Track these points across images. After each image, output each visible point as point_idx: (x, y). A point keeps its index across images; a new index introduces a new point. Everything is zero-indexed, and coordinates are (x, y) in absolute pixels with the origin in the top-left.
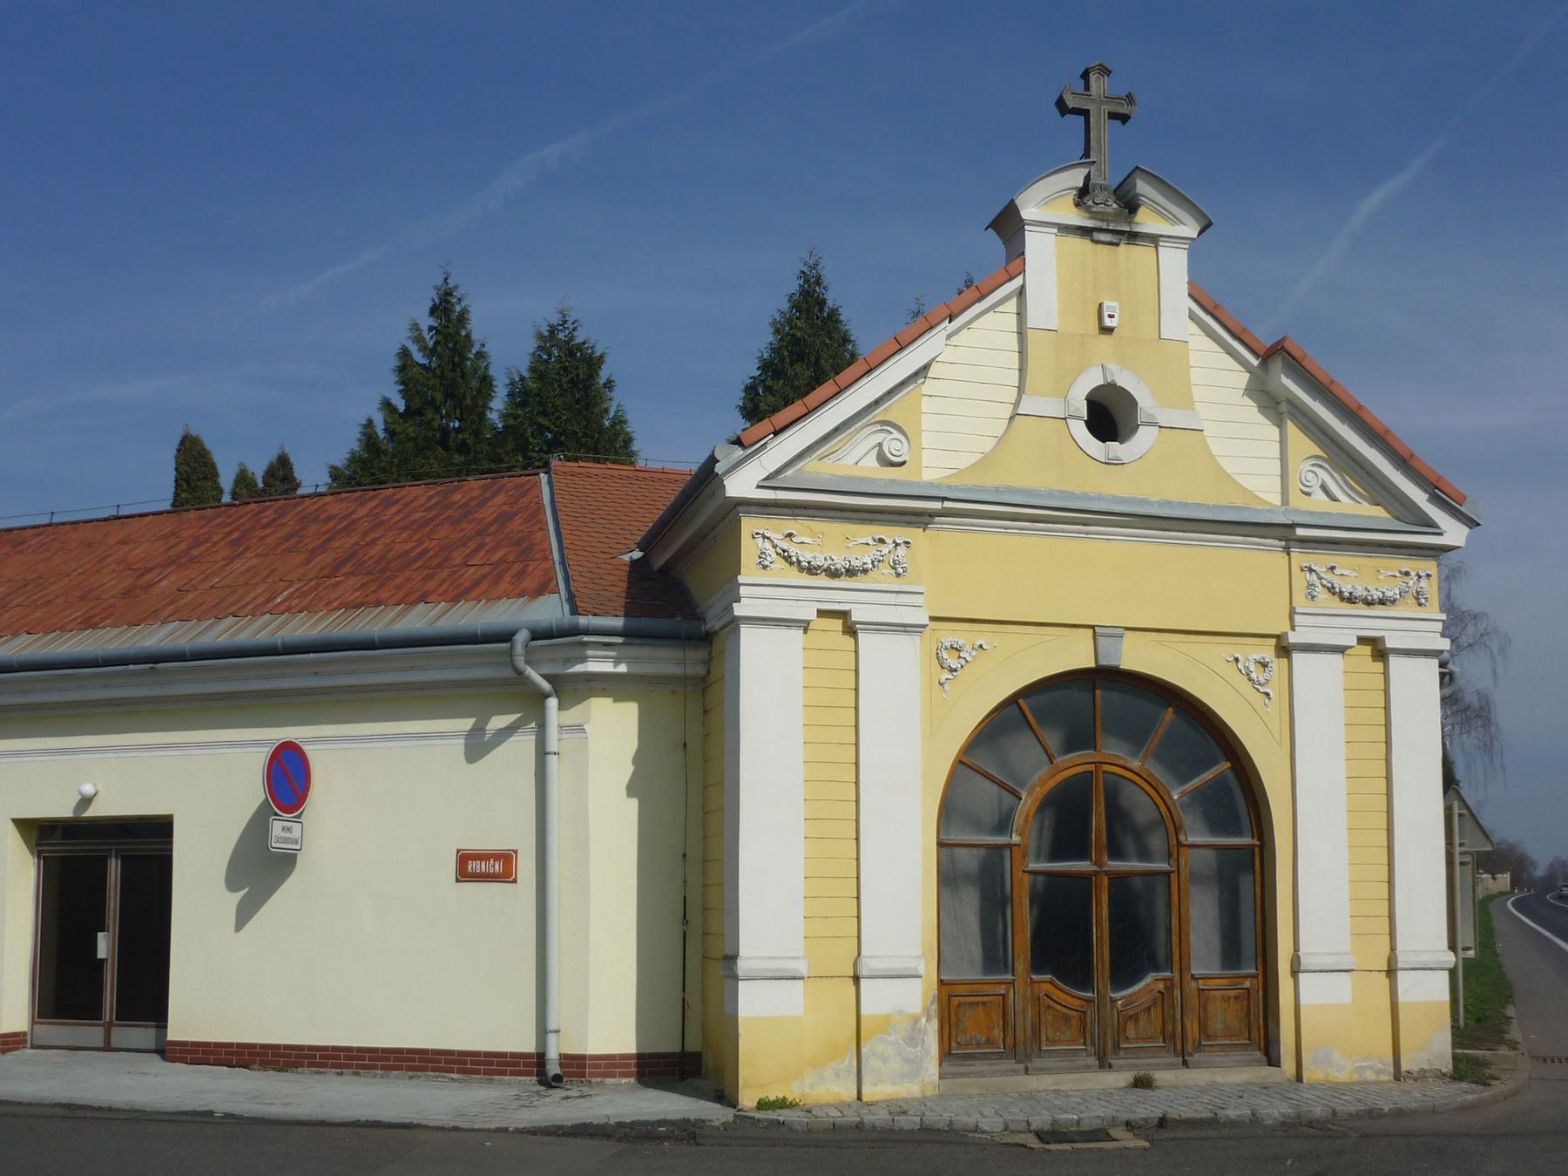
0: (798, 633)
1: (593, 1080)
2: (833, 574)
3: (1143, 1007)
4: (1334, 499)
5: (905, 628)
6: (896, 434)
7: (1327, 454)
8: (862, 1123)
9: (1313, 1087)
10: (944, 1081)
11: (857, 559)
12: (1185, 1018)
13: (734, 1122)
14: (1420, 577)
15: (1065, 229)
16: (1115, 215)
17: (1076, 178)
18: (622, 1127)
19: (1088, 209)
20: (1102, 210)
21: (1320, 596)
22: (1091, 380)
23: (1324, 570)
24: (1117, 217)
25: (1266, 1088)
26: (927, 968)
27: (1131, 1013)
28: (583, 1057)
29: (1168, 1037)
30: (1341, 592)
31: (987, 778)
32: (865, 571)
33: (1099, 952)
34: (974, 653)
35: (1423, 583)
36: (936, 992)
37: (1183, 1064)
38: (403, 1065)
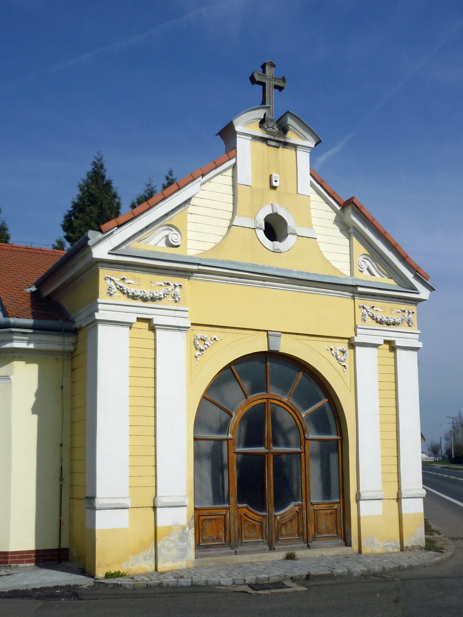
0: (126, 329)
1: (12, 565)
2: (145, 299)
3: (289, 519)
4: (372, 275)
5: (179, 328)
6: (175, 231)
7: (369, 253)
8: (161, 583)
9: (367, 556)
10: (198, 560)
11: (156, 292)
12: (308, 524)
13: (94, 585)
14: (409, 313)
15: (255, 138)
16: (277, 133)
17: (260, 114)
18: (36, 591)
19: (265, 129)
20: (271, 130)
21: (368, 320)
22: (266, 211)
23: (369, 308)
24: (278, 135)
25: (346, 557)
26: (189, 502)
27: (283, 522)
28: (7, 553)
29: (300, 534)
30: (377, 319)
31: (217, 406)
32: (160, 299)
33: (269, 492)
34: (212, 342)
35: (411, 316)
36: (193, 514)
37: (308, 547)
38: (24, 560)
